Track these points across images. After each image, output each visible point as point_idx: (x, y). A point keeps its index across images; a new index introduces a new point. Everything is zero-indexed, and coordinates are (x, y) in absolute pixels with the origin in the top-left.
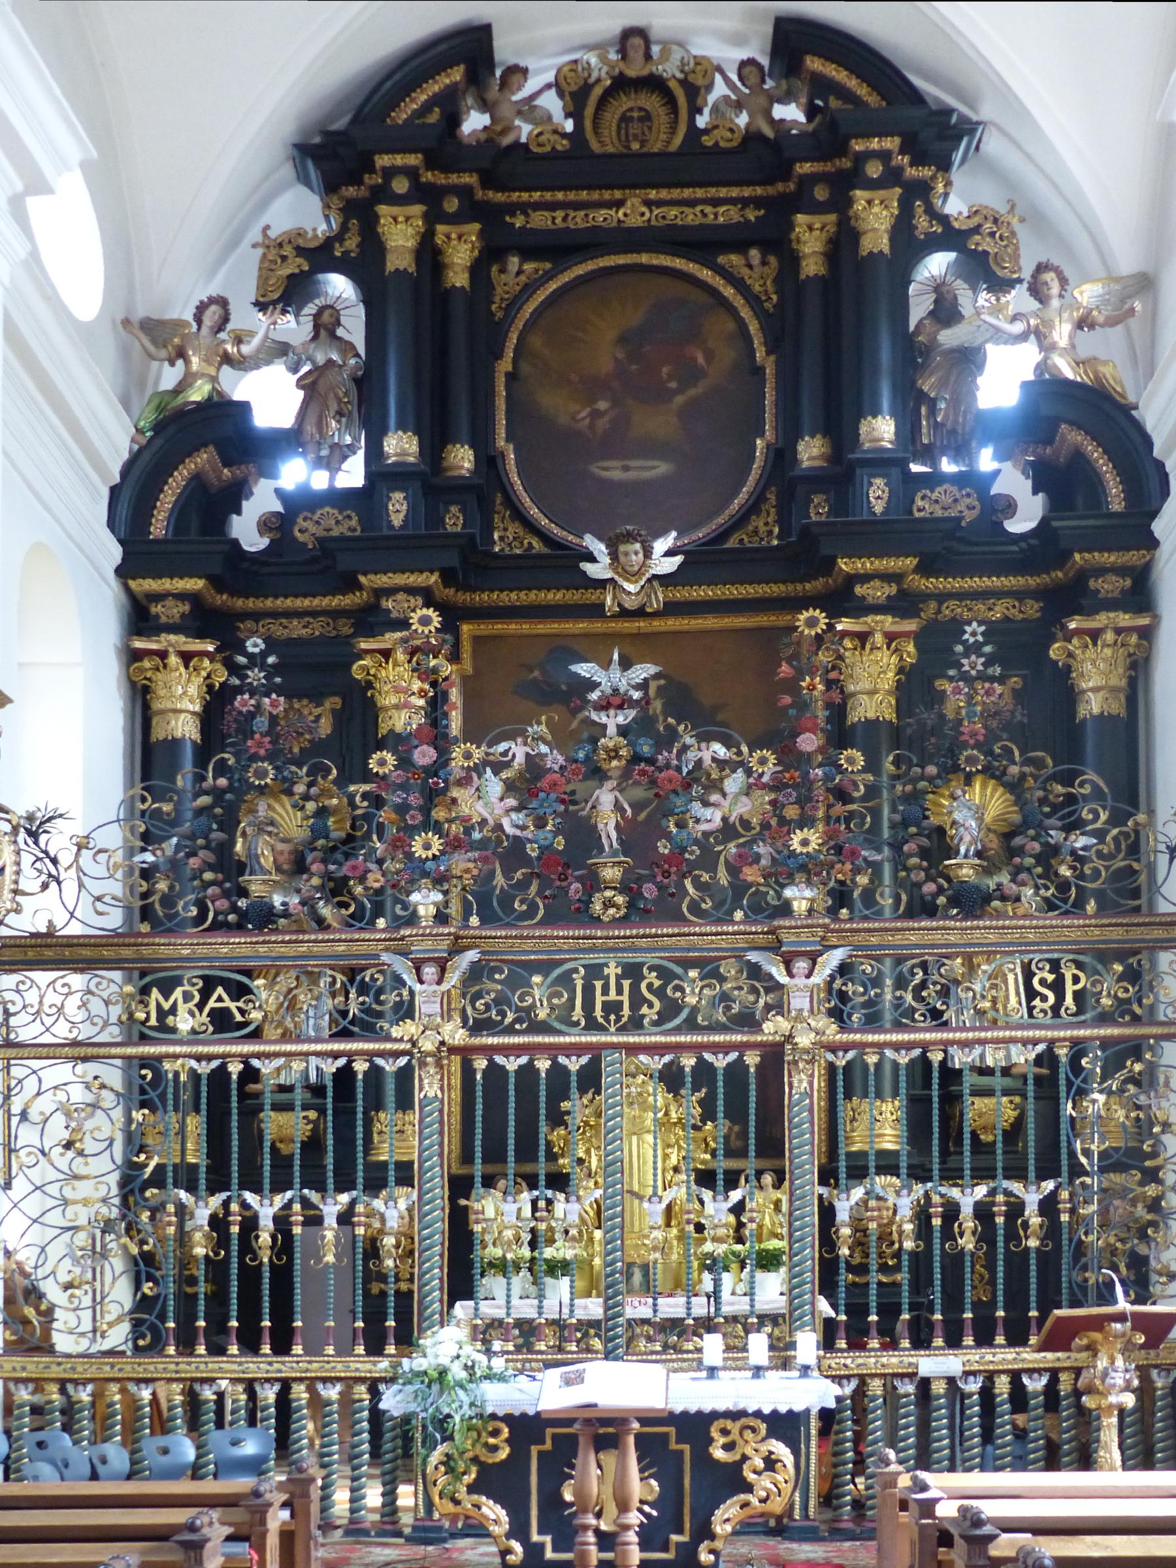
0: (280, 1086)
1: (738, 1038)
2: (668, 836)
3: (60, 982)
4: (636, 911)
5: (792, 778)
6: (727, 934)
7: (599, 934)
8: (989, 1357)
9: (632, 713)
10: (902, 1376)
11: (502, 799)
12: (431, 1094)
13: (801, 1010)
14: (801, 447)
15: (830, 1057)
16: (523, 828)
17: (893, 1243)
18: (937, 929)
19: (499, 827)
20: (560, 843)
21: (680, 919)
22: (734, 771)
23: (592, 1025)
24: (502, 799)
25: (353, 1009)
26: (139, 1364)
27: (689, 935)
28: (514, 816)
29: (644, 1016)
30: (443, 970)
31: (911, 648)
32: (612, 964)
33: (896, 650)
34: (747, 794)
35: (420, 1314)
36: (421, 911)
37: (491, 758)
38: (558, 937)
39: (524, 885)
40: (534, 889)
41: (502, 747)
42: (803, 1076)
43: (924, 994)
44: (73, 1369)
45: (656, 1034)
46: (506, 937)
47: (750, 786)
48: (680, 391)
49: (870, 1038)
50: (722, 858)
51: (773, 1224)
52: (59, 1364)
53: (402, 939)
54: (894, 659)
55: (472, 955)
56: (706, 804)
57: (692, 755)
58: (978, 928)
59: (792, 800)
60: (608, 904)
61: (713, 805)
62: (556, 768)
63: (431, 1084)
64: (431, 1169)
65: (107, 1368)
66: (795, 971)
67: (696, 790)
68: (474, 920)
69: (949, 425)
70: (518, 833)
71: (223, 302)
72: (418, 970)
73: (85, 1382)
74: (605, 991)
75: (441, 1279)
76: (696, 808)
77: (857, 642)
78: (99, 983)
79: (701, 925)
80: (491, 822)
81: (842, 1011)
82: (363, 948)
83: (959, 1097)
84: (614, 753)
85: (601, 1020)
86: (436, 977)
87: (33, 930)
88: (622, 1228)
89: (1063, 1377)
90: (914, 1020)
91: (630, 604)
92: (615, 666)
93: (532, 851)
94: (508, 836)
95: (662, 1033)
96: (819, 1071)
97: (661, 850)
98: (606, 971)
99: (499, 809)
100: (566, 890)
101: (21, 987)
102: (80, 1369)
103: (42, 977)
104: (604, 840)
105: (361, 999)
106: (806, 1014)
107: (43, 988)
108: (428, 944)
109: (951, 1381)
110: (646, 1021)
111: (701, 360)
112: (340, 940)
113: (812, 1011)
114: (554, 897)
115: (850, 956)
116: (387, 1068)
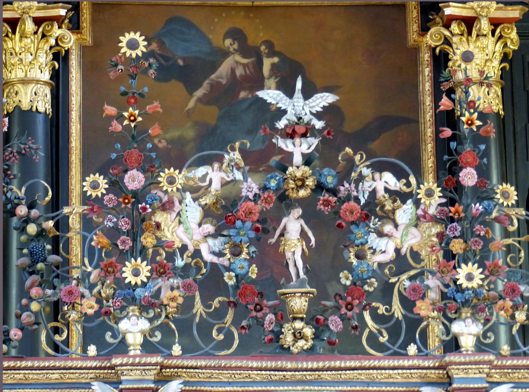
2: (350, 268)
5: (457, 212)
7: (289, 365)
9: (314, 142)
11: (200, 225)
16: (220, 254)
19: (197, 253)
20: (253, 272)
22: (404, 202)
24: (200, 225)
27: (369, 368)
28: (210, 241)
31: (514, 35)
33: (500, 37)
34: (416, 226)
36: (130, 339)
37: (191, 183)
38: (252, 369)
39: (219, 314)
40: (229, 317)
41: (201, 171)
46: (206, 368)
47: (418, 218)
53: (112, 368)
54: (499, 47)
56: (381, 234)
57: (367, 186)
59: (457, 234)
61: (387, 235)
62: (251, 196)
67: (374, 222)
68: (177, 350)
70: (215, 259)
71: (337, 294)
76: (373, 240)
77: (464, 27)
79: (379, 359)
84: (301, 183)
90: (500, 356)
92: (298, 95)
93: (230, 279)
94: (205, 263)
97: (343, 281)
99: (198, 233)
100: (260, 323)
108: (136, 374)
112: (54, 368)
114: (249, 327)
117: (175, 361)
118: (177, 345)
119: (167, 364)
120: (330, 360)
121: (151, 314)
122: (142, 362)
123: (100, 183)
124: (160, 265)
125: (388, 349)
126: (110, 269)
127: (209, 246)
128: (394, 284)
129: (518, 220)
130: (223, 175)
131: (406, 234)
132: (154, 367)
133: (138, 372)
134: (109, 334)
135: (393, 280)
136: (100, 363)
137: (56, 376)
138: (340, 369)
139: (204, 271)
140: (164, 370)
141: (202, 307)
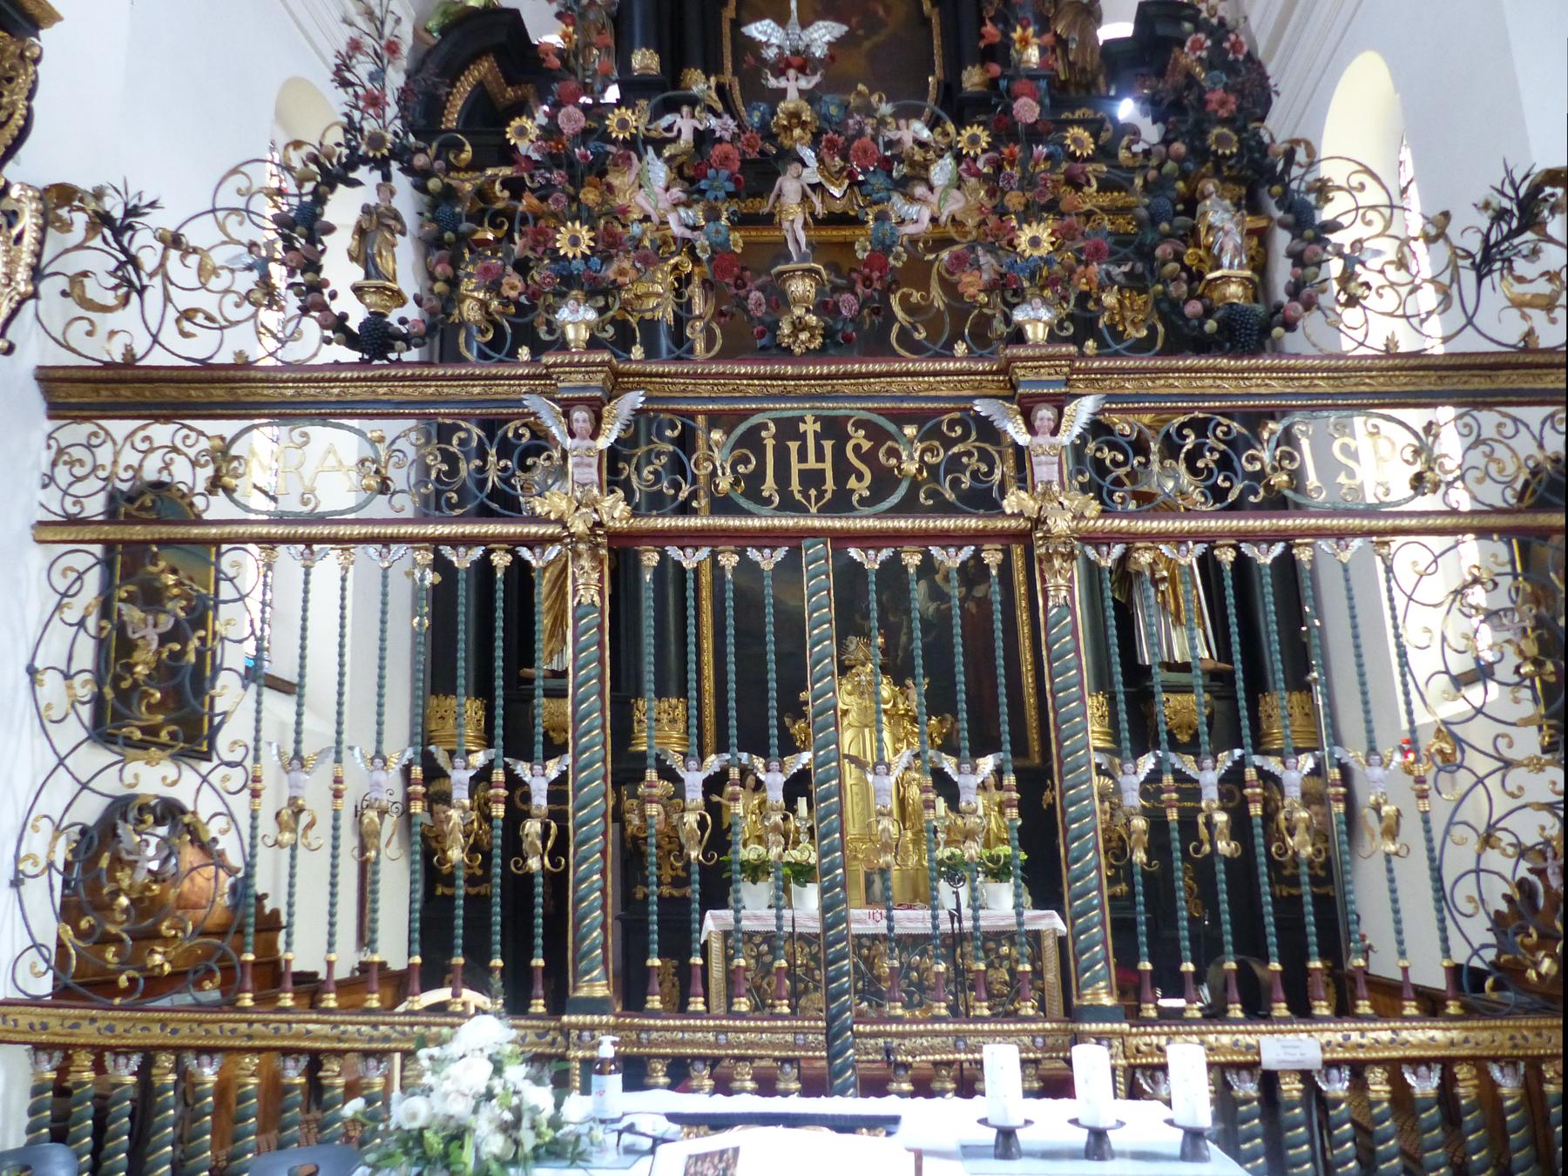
0: (552, 671)
1: (972, 523)
3: (141, 434)
4: (834, 342)
6: (948, 373)
7: (790, 370)
8: (1355, 1037)
10: (1238, 1067)
11: (667, 189)
12: (586, 600)
13: (1050, 482)
14: (965, 75)
15: (1091, 552)
17: (1201, 843)
18: (1207, 370)
21: (890, 354)
22: (941, 157)
23: (789, 505)
24: (667, 189)
25: (493, 477)
26: (200, 1023)
28: (682, 211)
29: (852, 491)
30: (598, 419)
32: (809, 418)
34: (959, 188)
35: (576, 949)
36: (571, 333)
37: (653, 134)
42: (1061, 581)
43: (1200, 464)
44: (111, 1028)
45: (867, 517)
46: (676, 375)
48: (867, 37)
49: (1142, 525)
50: (935, 270)
51: (999, 828)
52: (93, 1020)
55: (635, 399)
56: (912, 199)
58: (1257, 369)
60: (799, 326)
62: (727, 136)
63: (587, 585)
64: (588, 714)
65: (156, 1029)
66: (1037, 423)
69: (1080, 65)
72: (566, 415)
73: (128, 1051)
74: (803, 457)
75: (603, 891)
78: (187, 437)
79: (914, 361)
80: (655, 219)
81: (1100, 488)
82: (501, 390)
83: (1150, 695)
85: (798, 496)
86: (588, 427)
87: (107, 359)
88: (841, 814)
89: (1462, 1072)
91: (838, 207)
95: (877, 516)
96: (1076, 571)
98: (802, 427)
99: (665, 201)
101: (94, 441)
102: (119, 1029)
103: (119, 428)
104: (791, 247)
105: (502, 463)
106: (1056, 488)
107: (120, 441)
108: (578, 379)
109: (1306, 1076)
110: (855, 498)
111: (881, 12)
113: (1062, 484)
115: (1103, 411)
116: (534, 563)
120: (846, 363)
121: (601, 303)
125: (928, 350)
128: (931, 263)
129: (1097, 179)
130: (696, 123)
131: (944, 198)
135: (931, 257)
137: (477, 390)
138: (860, 375)
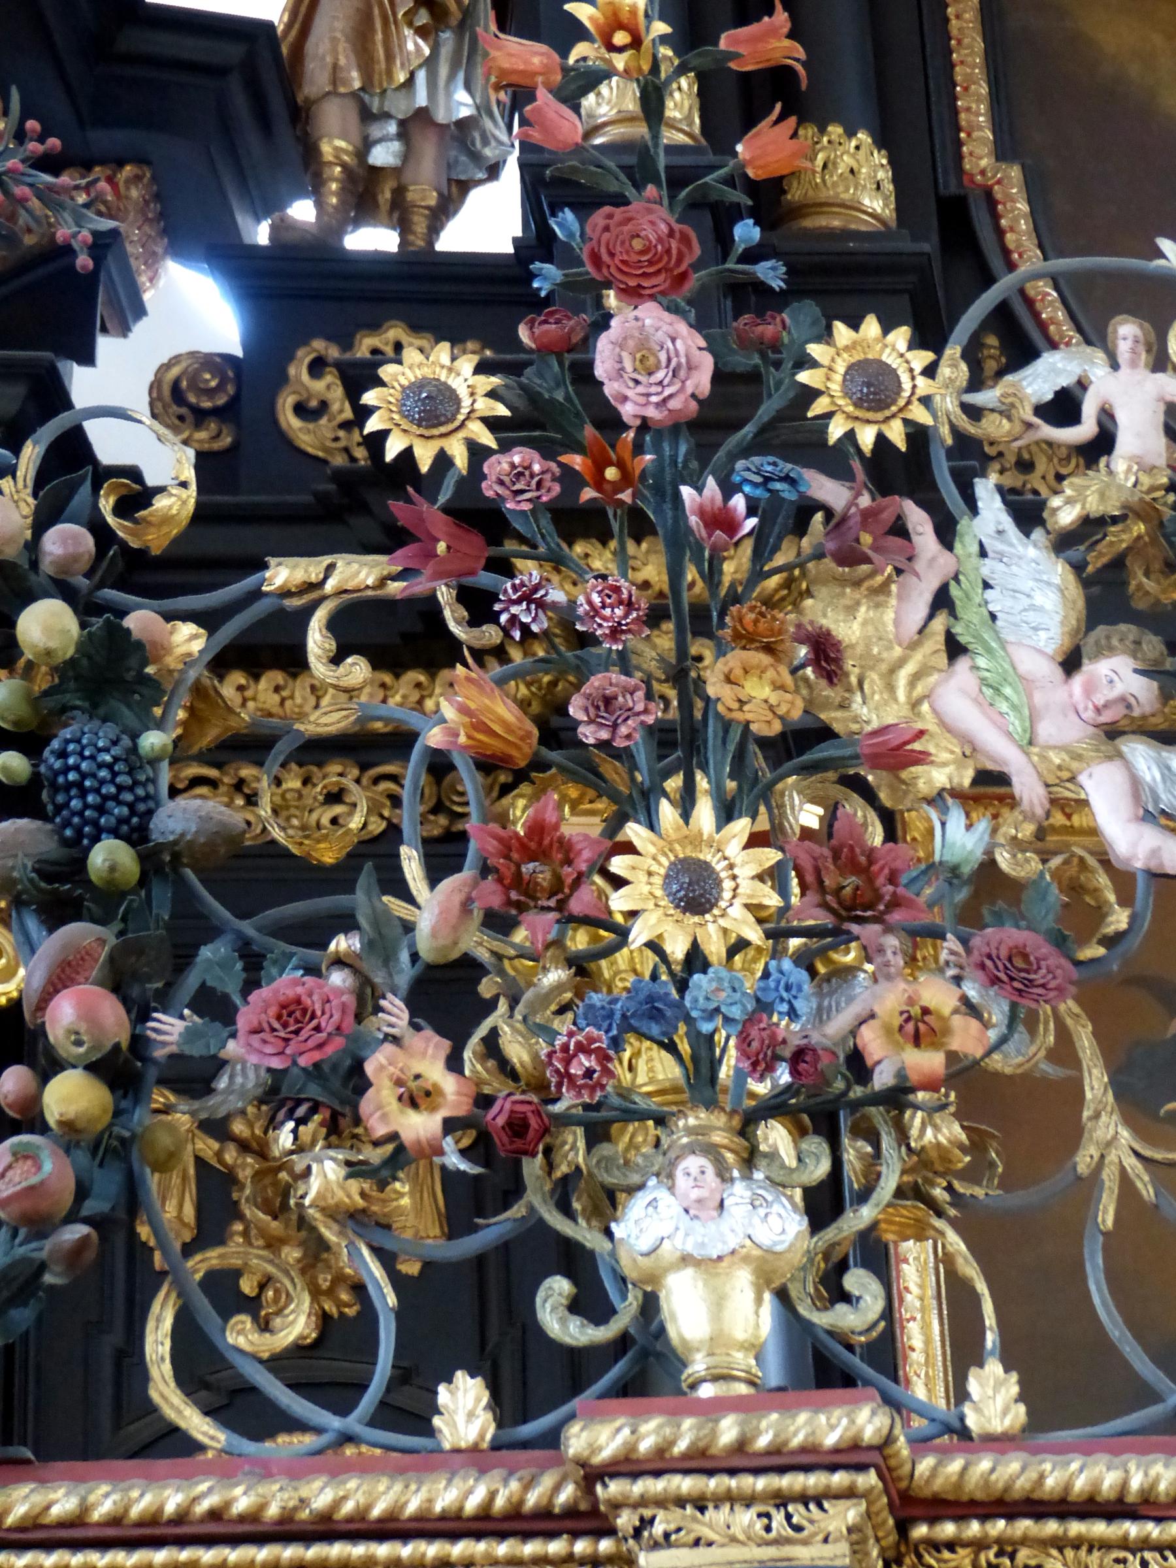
11: (1071, 663)
24: (1071, 663)
94: (1123, 879)
117: (985, 1464)
118: (994, 1367)
119: (938, 1485)
122: (762, 1442)
123: (463, 392)
124: (836, 854)
126: (539, 872)
127: (1135, 783)
132: (839, 1479)
133: (745, 1518)
134: (559, 1287)
136: (514, 1485)
139: (1119, 919)
140: (921, 1531)
141: (1125, 1134)
